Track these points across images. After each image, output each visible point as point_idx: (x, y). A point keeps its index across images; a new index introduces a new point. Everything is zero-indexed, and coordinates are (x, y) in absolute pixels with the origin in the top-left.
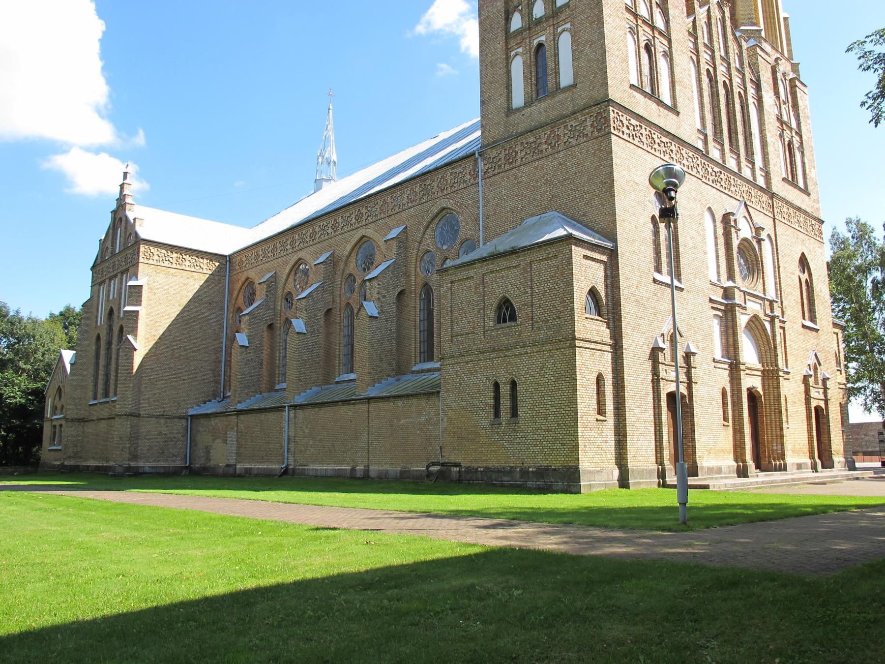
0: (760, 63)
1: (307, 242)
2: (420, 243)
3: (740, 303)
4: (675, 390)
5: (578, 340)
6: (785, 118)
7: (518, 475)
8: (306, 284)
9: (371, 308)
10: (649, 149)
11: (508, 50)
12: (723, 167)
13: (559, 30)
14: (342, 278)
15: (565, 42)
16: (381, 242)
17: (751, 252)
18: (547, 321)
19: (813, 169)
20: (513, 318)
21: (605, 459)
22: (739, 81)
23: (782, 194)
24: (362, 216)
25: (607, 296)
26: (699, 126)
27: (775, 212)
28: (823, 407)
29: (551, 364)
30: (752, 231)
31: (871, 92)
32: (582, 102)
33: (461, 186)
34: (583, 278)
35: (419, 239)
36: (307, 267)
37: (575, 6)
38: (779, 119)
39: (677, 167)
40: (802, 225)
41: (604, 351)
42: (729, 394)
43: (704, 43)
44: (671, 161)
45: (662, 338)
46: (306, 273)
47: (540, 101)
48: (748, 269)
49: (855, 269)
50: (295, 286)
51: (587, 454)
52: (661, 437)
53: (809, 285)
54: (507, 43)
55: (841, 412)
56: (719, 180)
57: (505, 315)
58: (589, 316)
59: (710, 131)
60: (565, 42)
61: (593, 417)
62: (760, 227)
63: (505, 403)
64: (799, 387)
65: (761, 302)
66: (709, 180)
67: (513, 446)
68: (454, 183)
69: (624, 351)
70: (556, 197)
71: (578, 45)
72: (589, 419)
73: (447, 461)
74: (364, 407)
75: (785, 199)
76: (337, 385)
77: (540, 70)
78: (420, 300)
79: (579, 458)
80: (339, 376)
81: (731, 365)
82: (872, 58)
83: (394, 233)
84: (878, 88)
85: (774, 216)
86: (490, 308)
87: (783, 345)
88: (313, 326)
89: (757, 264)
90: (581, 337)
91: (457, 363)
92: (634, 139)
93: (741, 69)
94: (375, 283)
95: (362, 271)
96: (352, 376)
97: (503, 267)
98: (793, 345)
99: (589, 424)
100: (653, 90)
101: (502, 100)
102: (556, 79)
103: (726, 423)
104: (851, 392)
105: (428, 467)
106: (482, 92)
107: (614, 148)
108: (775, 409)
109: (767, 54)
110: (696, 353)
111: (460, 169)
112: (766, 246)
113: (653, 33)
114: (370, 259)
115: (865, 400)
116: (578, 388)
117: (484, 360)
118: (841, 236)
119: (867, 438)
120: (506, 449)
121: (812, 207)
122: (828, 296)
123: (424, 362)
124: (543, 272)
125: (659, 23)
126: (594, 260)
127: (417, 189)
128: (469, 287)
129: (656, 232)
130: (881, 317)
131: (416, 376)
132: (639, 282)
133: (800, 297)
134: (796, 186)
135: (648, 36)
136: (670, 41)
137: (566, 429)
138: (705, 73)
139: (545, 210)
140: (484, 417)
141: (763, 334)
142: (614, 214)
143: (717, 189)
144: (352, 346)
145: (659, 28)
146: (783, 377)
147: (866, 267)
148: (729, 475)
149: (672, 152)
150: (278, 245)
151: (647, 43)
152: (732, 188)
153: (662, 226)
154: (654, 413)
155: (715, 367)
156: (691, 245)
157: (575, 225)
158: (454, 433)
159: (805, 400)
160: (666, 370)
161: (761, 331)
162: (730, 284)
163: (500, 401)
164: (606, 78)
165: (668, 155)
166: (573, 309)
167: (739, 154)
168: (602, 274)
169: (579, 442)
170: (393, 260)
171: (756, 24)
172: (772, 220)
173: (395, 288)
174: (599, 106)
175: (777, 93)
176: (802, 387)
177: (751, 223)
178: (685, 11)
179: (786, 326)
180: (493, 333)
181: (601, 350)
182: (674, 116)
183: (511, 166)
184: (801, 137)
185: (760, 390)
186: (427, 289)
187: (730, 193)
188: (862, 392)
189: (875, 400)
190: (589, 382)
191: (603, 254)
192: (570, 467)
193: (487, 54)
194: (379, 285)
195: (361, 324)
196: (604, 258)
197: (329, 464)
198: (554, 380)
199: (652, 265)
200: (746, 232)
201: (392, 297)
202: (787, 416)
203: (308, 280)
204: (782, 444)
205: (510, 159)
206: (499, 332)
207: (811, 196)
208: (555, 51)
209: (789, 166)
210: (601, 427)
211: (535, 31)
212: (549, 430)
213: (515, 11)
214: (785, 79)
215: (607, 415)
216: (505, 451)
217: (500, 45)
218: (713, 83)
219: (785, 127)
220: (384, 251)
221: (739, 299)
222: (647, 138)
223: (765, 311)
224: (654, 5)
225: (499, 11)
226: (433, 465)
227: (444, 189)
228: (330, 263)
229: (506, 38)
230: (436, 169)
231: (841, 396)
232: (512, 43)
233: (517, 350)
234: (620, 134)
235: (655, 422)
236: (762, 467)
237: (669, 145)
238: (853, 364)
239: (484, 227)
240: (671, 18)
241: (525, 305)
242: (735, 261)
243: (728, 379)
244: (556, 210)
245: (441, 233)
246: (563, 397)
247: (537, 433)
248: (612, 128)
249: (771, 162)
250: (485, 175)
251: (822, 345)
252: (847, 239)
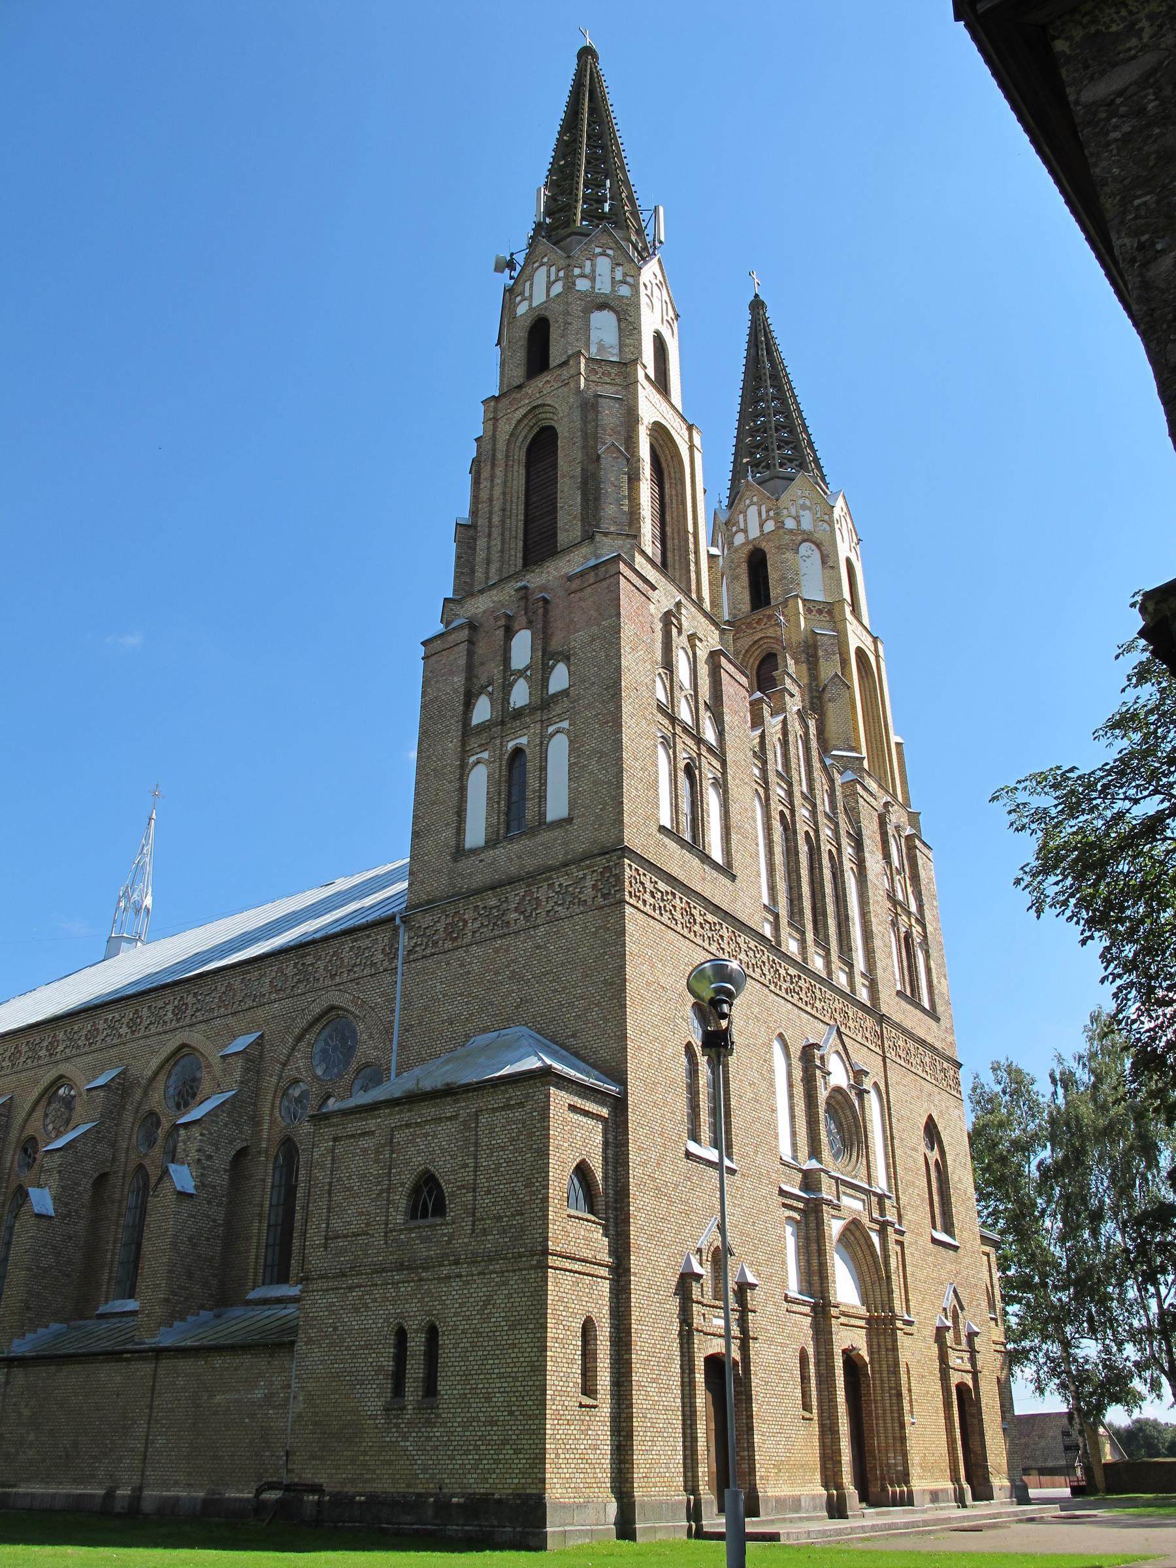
0: (861, 808)
1: (78, 1047)
2: (284, 1065)
3: (830, 1198)
4: (724, 1351)
5: (552, 1254)
6: (900, 897)
7: (430, 1512)
8: (68, 1123)
9: (183, 1177)
10: (685, 932)
11: (464, 753)
12: (804, 969)
13: (551, 729)
14: (135, 1119)
15: (559, 750)
16: (214, 1058)
17: (848, 1112)
18: (499, 1219)
19: (943, 979)
20: (440, 1210)
21: (593, 1480)
22: (829, 833)
23: (896, 1017)
24: (186, 1009)
25: (605, 1178)
26: (765, 900)
27: (886, 1045)
28: (971, 1384)
29: (501, 1297)
30: (848, 1077)
31: (1028, 865)
32: (580, 848)
33: (365, 972)
34: (566, 1145)
35: (283, 1058)
36: (73, 1093)
37: (578, 695)
38: (891, 897)
39: (734, 965)
40: (927, 1069)
41: (597, 1277)
42: (812, 1360)
43: (777, 771)
44: (720, 955)
45: (698, 1257)
46: (68, 1102)
47: (511, 840)
48: (843, 1140)
49: (1012, 1146)
50: (45, 1126)
51: (560, 1471)
52: (694, 1439)
53: (942, 1169)
54: (464, 743)
55: (1000, 1394)
56: (797, 989)
57: (425, 1203)
58: (573, 1212)
59: (783, 912)
60: (559, 750)
61: (574, 1399)
62: (862, 1070)
63: (415, 1369)
64: (929, 1348)
65: (864, 1197)
66: (780, 989)
67: (425, 1453)
68: (355, 965)
69: (632, 1278)
70: (527, 1001)
71: (579, 756)
72: (566, 1403)
73: (296, 1480)
74: (146, 1368)
75: (900, 1026)
76: (100, 1321)
77: (515, 790)
78: (274, 1168)
79: (545, 1479)
80: (106, 1302)
81: (814, 1308)
82: (1027, 813)
83: (240, 1044)
84: (1037, 859)
85: (884, 1052)
86: (400, 1189)
87: (901, 1274)
88: (68, 1204)
89: (858, 1133)
90: (558, 1249)
91: (332, 1289)
92: (661, 915)
93: (832, 816)
94: (195, 1131)
95: (175, 1108)
96: (132, 1305)
97: (429, 1118)
98: (920, 1275)
99: (566, 1412)
100: (694, 837)
101: (448, 833)
102: (540, 807)
103: (807, 1415)
104: (1014, 1358)
105: (259, 1491)
106: (415, 817)
107: (629, 927)
108: (890, 1389)
109: (871, 794)
110: (756, 1285)
111: (367, 942)
112: (873, 1102)
113: (699, 749)
114: (192, 1087)
115: (1037, 1372)
116: (548, 1344)
117: (382, 1285)
118: (987, 1089)
119: (1043, 1443)
120: (411, 1458)
121: (943, 1040)
122: (971, 1190)
123: (271, 1284)
124: (497, 1130)
125: (710, 735)
126: (586, 1114)
127: (290, 971)
128: (364, 1151)
129: (693, 1071)
130: (1055, 1227)
131: (253, 1310)
132: (662, 1157)
133: (926, 1190)
134: (918, 1006)
135: (691, 752)
136: (724, 763)
137: (523, 1422)
138: (778, 817)
139: (508, 1022)
140: (374, 1395)
141: (867, 1252)
142: (624, 1037)
143: (793, 1004)
144: (139, 1246)
145: (708, 742)
146: (901, 1330)
147: (1027, 1142)
148: (813, 1514)
149: (723, 940)
150: (24, 1048)
151: (688, 763)
152: (818, 1004)
153: (702, 1060)
154: (683, 1394)
155: (787, 1311)
156: (750, 1095)
157: (558, 1052)
158: (316, 1424)
159: (940, 1371)
160: (704, 1315)
161: (865, 1247)
162: (813, 1164)
163: (405, 1365)
164: (621, 813)
165: (716, 944)
166: (546, 1199)
167: (829, 949)
168: (599, 1139)
169: (548, 1446)
170: (233, 1092)
171: (856, 749)
172: (881, 1058)
173: (231, 1143)
174: (607, 856)
175: (887, 856)
176: (935, 1348)
177: (847, 1063)
178: (749, 719)
179: (906, 1239)
180: (402, 1237)
181: (592, 1276)
182: (727, 882)
183: (455, 944)
184: (924, 927)
185: (864, 1353)
186: (289, 1149)
187: (814, 1012)
188: (1032, 1357)
189: (1054, 1373)
190: (568, 1333)
191: (603, 1104)
192: (529, 1496)
193: (429, 757)
194: (202, 1135)
195: (161, 1209)
196: (605, 1112)
197: (60, 1483)
198: (506, 1328)
199: (685, 1128)
201: (222, 1160)
202: (911, 1401)
203: (70, 1116)
204: (905, 1454)
205: (453, 932)
206: (413, 1235)
207: (942, 1022)
208: (541, 762)
209: (906, 973)
210: (587, 1418)
211: (512, 728)
212: (493, 1423)
213: (481, 693)
214: (900, 836)
215: (599, 1396)
216: (408, 1462)
217: (452, 744)
218: (790, 833)
219: (899, 909)
220: (218, 1073)
221: (827, 1191)
222: (682, 914)
223: (870, 1214)
224: (702, 707)
225: (455, 691)
226: (269, 1489)
227: (336, 974)
228: (117, 1089)
229: (463, 733)
230: (326, 939)
231: (998, 1364)
232: (473, 743)
233: (443, 1268)
234: (640, 905)
235: (683, 1411)
236: (871, 1497)
237: (718, 927)
238: (1014, 1308)
239: (400, 1045)
240: (727, 728)
241: (463, 1187)
242: (822, 1126)
243: (811, 1332)
244: (526, 1024)
245: (324, 1051)
246: (522, 1359)
247: (471, 1428)
248: (626, 893)
249: (879, 964)
250: (408, 955)
251: (964, 1273)
252: (997, 1094)
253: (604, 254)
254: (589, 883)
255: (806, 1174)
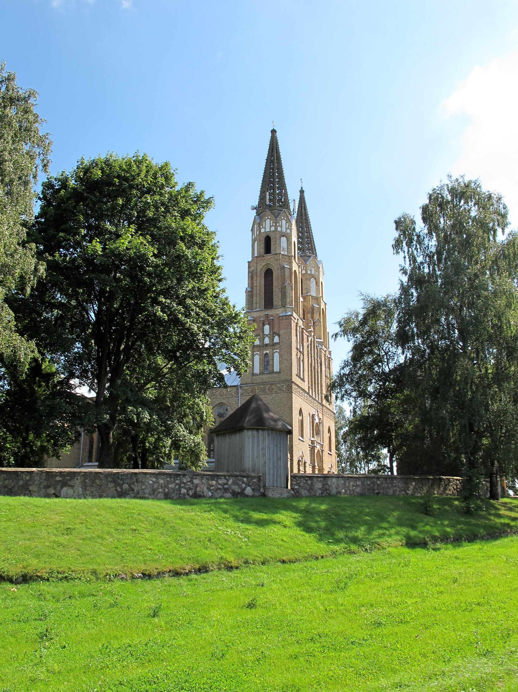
6: (299, 348)
13: (275, 351)
15: (276, 356)
60: (276, 356)
192: (44, 464)
200: (317, 421)
253: (284, 219)
254: (285, 387)
255: (312, 441)
